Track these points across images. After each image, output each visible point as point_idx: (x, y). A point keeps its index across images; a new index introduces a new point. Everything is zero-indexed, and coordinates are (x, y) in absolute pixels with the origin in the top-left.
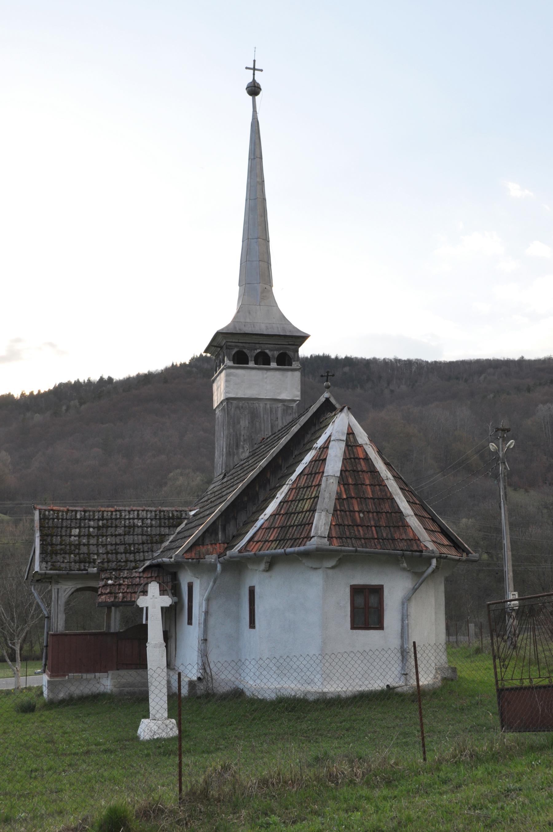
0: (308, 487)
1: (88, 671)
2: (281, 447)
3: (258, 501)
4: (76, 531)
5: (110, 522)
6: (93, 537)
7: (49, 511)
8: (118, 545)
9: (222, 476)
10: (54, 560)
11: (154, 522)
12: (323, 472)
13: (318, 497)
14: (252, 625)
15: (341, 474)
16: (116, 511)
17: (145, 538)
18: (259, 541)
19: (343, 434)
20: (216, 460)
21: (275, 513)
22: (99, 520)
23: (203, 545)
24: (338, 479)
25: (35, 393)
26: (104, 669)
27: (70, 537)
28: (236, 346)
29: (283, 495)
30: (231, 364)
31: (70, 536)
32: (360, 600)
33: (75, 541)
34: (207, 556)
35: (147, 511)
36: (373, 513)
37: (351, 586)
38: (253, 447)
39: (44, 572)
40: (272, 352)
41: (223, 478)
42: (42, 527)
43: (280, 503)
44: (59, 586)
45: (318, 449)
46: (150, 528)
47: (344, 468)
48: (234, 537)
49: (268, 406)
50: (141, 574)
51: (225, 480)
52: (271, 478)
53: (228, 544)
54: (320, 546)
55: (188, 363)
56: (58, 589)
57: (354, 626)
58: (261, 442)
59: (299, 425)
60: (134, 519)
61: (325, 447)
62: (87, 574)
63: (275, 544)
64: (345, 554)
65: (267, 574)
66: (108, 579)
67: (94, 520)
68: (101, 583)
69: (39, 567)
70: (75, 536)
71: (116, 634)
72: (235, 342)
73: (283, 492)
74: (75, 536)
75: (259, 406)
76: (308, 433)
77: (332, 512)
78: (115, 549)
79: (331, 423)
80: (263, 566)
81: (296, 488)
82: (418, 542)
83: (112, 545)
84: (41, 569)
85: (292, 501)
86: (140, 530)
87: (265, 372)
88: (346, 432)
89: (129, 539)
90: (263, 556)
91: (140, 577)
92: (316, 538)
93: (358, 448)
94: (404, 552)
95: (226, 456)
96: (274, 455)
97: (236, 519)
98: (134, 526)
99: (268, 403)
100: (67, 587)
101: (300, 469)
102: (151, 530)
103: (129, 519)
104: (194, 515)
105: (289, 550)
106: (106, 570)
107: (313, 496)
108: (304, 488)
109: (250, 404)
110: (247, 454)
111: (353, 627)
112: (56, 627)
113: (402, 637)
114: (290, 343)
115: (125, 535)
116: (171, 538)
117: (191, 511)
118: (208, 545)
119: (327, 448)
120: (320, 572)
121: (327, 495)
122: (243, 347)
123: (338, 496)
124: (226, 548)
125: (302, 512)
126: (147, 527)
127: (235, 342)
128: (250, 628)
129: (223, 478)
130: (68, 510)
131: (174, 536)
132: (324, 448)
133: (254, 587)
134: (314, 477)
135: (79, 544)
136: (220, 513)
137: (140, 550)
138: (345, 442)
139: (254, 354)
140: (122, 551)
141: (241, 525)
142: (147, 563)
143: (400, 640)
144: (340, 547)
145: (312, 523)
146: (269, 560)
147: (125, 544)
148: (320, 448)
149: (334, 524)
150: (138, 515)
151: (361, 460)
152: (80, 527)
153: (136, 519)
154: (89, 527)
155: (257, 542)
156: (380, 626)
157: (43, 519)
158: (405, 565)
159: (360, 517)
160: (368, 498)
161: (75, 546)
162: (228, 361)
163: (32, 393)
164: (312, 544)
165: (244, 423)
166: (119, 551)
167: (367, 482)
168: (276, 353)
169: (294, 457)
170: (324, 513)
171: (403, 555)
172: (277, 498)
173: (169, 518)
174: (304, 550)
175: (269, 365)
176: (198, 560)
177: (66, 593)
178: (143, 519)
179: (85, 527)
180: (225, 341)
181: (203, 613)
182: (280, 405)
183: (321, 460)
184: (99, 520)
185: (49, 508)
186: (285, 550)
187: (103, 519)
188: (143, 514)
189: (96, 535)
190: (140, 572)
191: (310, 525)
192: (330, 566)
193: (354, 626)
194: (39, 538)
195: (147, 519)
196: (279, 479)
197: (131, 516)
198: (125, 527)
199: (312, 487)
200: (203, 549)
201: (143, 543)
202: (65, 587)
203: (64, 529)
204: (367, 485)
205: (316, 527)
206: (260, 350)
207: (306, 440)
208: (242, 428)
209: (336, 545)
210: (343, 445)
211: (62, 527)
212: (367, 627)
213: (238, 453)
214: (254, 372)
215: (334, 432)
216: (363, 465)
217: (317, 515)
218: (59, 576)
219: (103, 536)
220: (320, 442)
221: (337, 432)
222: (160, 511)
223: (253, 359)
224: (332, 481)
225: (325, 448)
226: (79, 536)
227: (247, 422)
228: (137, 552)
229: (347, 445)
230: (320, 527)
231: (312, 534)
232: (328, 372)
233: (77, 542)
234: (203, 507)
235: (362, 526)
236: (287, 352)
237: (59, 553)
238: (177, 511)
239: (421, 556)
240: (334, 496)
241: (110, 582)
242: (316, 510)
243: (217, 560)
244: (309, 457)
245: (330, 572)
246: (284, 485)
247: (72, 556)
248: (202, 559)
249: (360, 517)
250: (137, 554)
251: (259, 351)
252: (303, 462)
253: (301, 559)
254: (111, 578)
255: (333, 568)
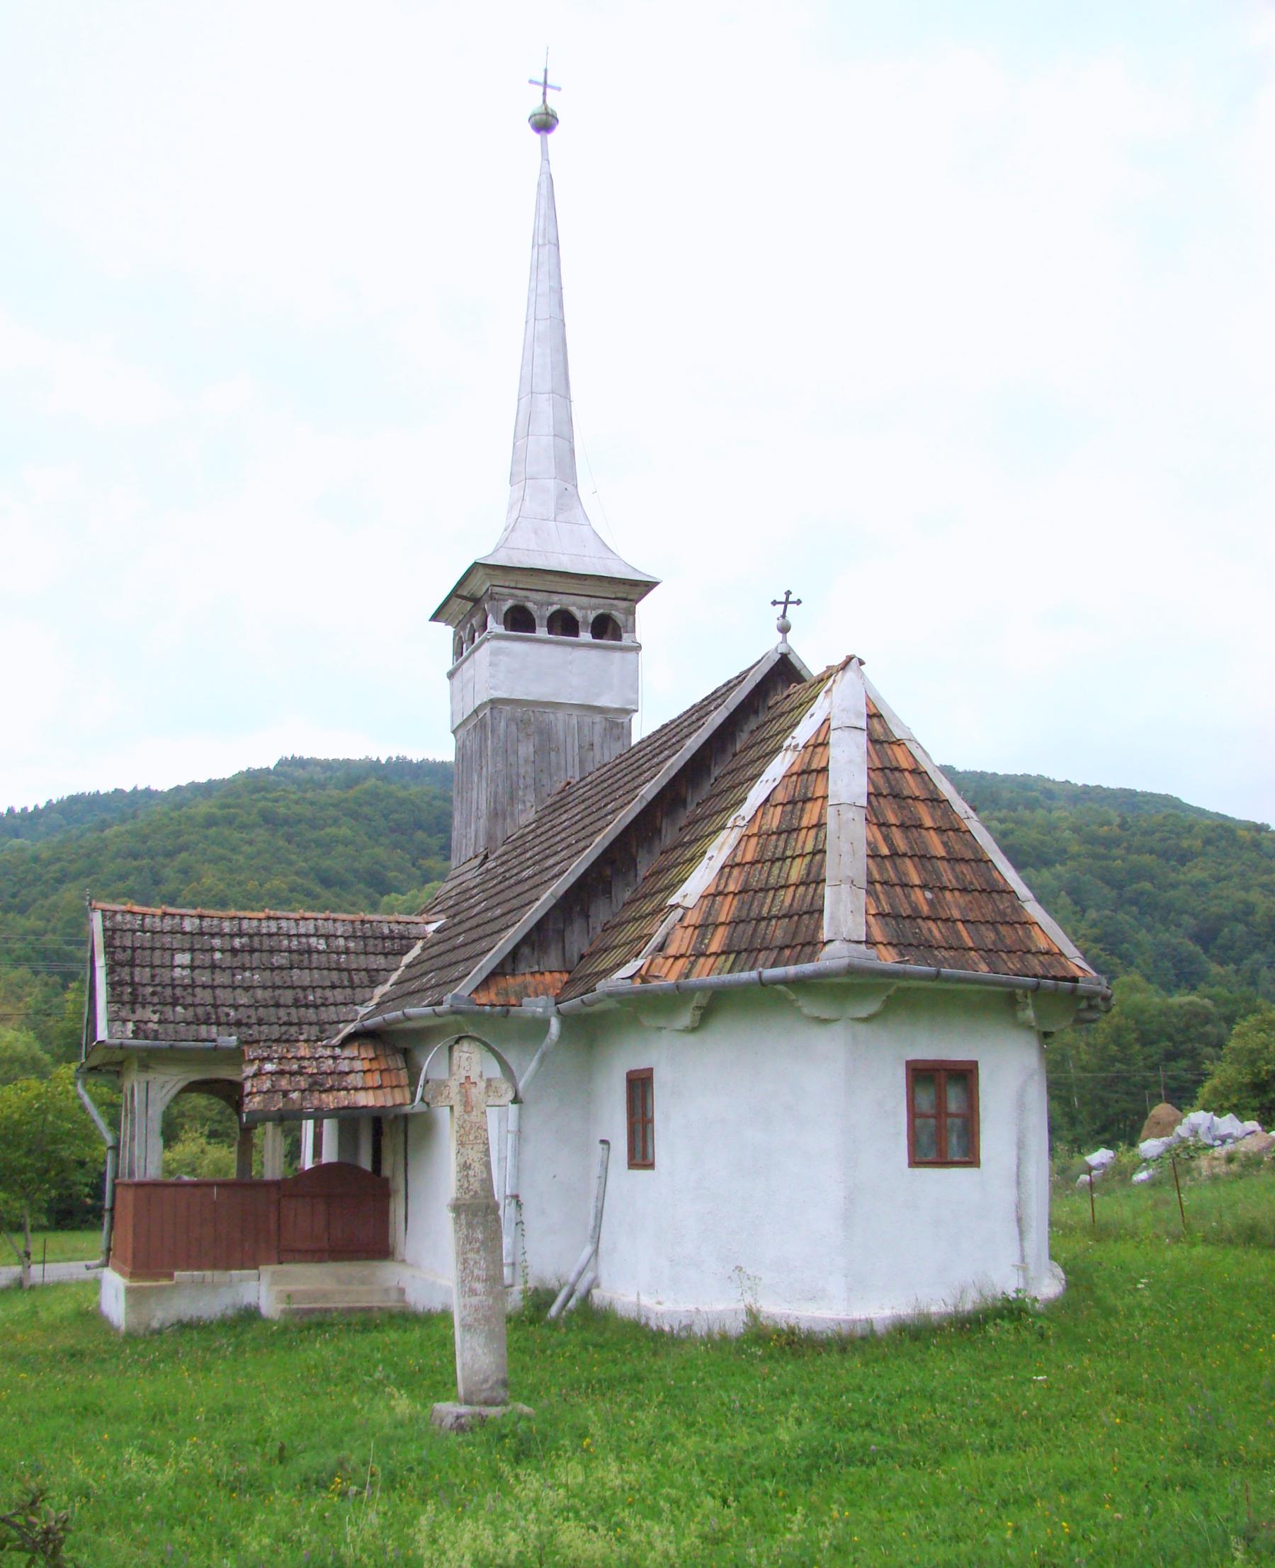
0: (790, 832)
1: (214, 1266)
2: (688, 756)
3: (636, 876)
4: (183, 958)
5: (256, 939)
6: (224, 969)
7: (124, 913)
8: (279, 987)
9: (477, 862)
10: (137, 1017)
11: (352, 945)
12: (825, 798)
13: (823, 851)
14: (640, 1156)
15: (869, 802)
16: (269, 918)
17: (335, 975)
18: (682, 956)
19: (858, 715)
20: (455, 834)
21: (712, 890)
22: (232, 936)
23: (513, 974)
24: (864, 811)
25: (31, 809)
26: (250, 1261)
27: (172, 970)
28: (512, 596)
29: (727, 851)
30: (500, 629)
31: (173, 967)
32: (926, 1100)
33: (183, 978)
34: (525, 1000)
35: (335, 920)
36: (951, 890)
37: (908, 1063)
38: (542, 801)
39: (118, 1041)
40: (584, 611)
41: (482, 864)
42: (108, 945)
43: (723, 868)
44: (150, 1076)
45: (799, 748)
46: (343, 956)
47: (872, 790)
48: (582, 957)
49: (574, 721)
50: (338, 1051)
51: (490, 865)
52: (664, 826)
53: (569, 972)
54: (856, 961)
55: (272, 767)
56: (148, 1083)
57: (916, 1161)
58: (563, 790)
59: (725, 710)
60: (308, 936)
61: (819, 744)
62: (216, 1048)
63: (725, 961)
64: (903, 984)
65: (692, 1038)
66: (264, 1060)
67: (222, 935)
68: (250, 1070)
69: (106, 1032)
70: (183, 967)
71: (277, 1184)
72: (509, 587)
73: (723, 844)
74: (183, 967)
75: (556, 719)
76: (742, 731)
77: (864, 885)
78: (273, 997)
79: (822, 694)
80: (686, 1018)
81: (759, 835)
82: (1063, 960)
83: (265, 988)
84: (111, 1035)
85: (753, 863)
86: (324, 958)
87: (569, 649)
88: (864, 711)
89: (303, 977)
90: (693, 990)
91: (335, 1058)
92: (837, 943)
93: (895, 747)
94: (1040, 980)
95: (489, 820)
96: (673, 773)
97: (588, 917)
98: (310, 951)
99: (575, 712)
100: (167, 1078)
101: (757, 794)
102: (347, 959)
103: (299, 936)
104: (437, 931)
105: (769, 973)
106: (258, 1042)
107: (809, 848)
108: (779, 833)
109: (537, 714)
110: (532, 816)
111: (915, 1162)
112: (143, 1167)
113: (1018, 1183)
114: (619, 595)
115: (291, 968)
116: (394, 977)
117: (428, 923)
118: (524, 974)
119: (825, 744)
120: (837, 1028)
121: (845, 847)
122: (526, 597)
123: (872, 850)
124: (566, 983)
125: (786, 887)
126: (338, 953)
127: (509, 587)
128: (629, 1168)
129: (482, 864)
130: (165, 914)
131: (399, 972)
132: (816, 746)
133: (651, 1070)
134: (802, 810)
135: (193, 985)
136: (554, 901)
137: (326, 999)
138: (865, 733)
139: (548, 614)
140: (290, 1002)
141: (599, 930)
142: (349, 1029)
143: (1014, 1191)
144: (902, 966)
145: (821, 911)
146: (704, 1002)
147: (294, 988)
148: (805, 747)
149: (873, 912)
150: (316, 928)
151: (906, 774)
152: (192, 950)
153: (313, 935)
154: (213, 950)
155: (676, 958)
156: (971, 1158)
157: (111, 933)
158: (1030, 1014)
159: (926, 899)
160: (936, 857)
161: (185, 987)
162: (495, 625)
163: (25, 809)
164: (833, 956)
165: (526, 750)
166: (282, 1001)
167: (928, 822)
168: (592, 616)
169: (712, 781)
170: (845, 888)
171: (1037, 988)
172: (710, 859)
173: (384, 938)
174: (815, 971)
175: (577, 635)
176: (505, 1008)
177: (165, 1091)
178: (327, 937)
179: (204, 951)
180: (488, 584)
181: (510, 1136)
182: (598, 718)
183: (813, 771)
184: (232, 936)
185: (123, 908)
186: (760, 973)
187: (240, 934)
188: (329, 927)
189: (229, 968)
190: (333, 1047)
191: (816, 915)
192: (864, 1014)
193: (916, 1161)
194: (104, 969)
195: (337, 937)
196: (680, 829)
197: (302, 931)
198: (290, 951)
199: (800, 830)
200: (511, 982)
201: (333, 987)
202: (162, 1078)
203: (158, 953)
204: (927, 829)
205: (832, 918)
206: (559, 607)
207: (738, 747)
208: (521, 762)
209: (887, 959)
210: (862, 738)
211: (153, 949)
212: (942, 1162)
213: (512, 814)
214: (546, 649)
215: (835, 712)
216: (911, 785)
217: (828, 892)
218: (151, 1052)
219: (244, 969)
220: (804, 732)
221: (843, 710)
222: (363, 922)
223: (545, 623)
224: (851, 815)
225: (820, 745)
226: (192, 968)
227: (531, 750)
228: (323, 1005)
229: (873, 741)
230: (842, 918)
231: (826, 934)
232: (788, 593)
233: (187, 981)
234: (454, 916)
235: (934, 920)
236: (613, 612)
237: (149, 1003)
238: (399, 923)
239: (1073, 991)
240: (863, 850)
241: (269, 1067)
242: (824, 881)
243: (554, 1009)
244: (778, 768)
245: (862, 1029)
246: (723, 828)
247: (179, 1009)
248: (514, 1005)
249: (926, 899)
250: (323, 1009)
251: (556, 607)
252: (763, 777)
253: (793, 997)
254: (269, 1059)
255: (867, 1020)
